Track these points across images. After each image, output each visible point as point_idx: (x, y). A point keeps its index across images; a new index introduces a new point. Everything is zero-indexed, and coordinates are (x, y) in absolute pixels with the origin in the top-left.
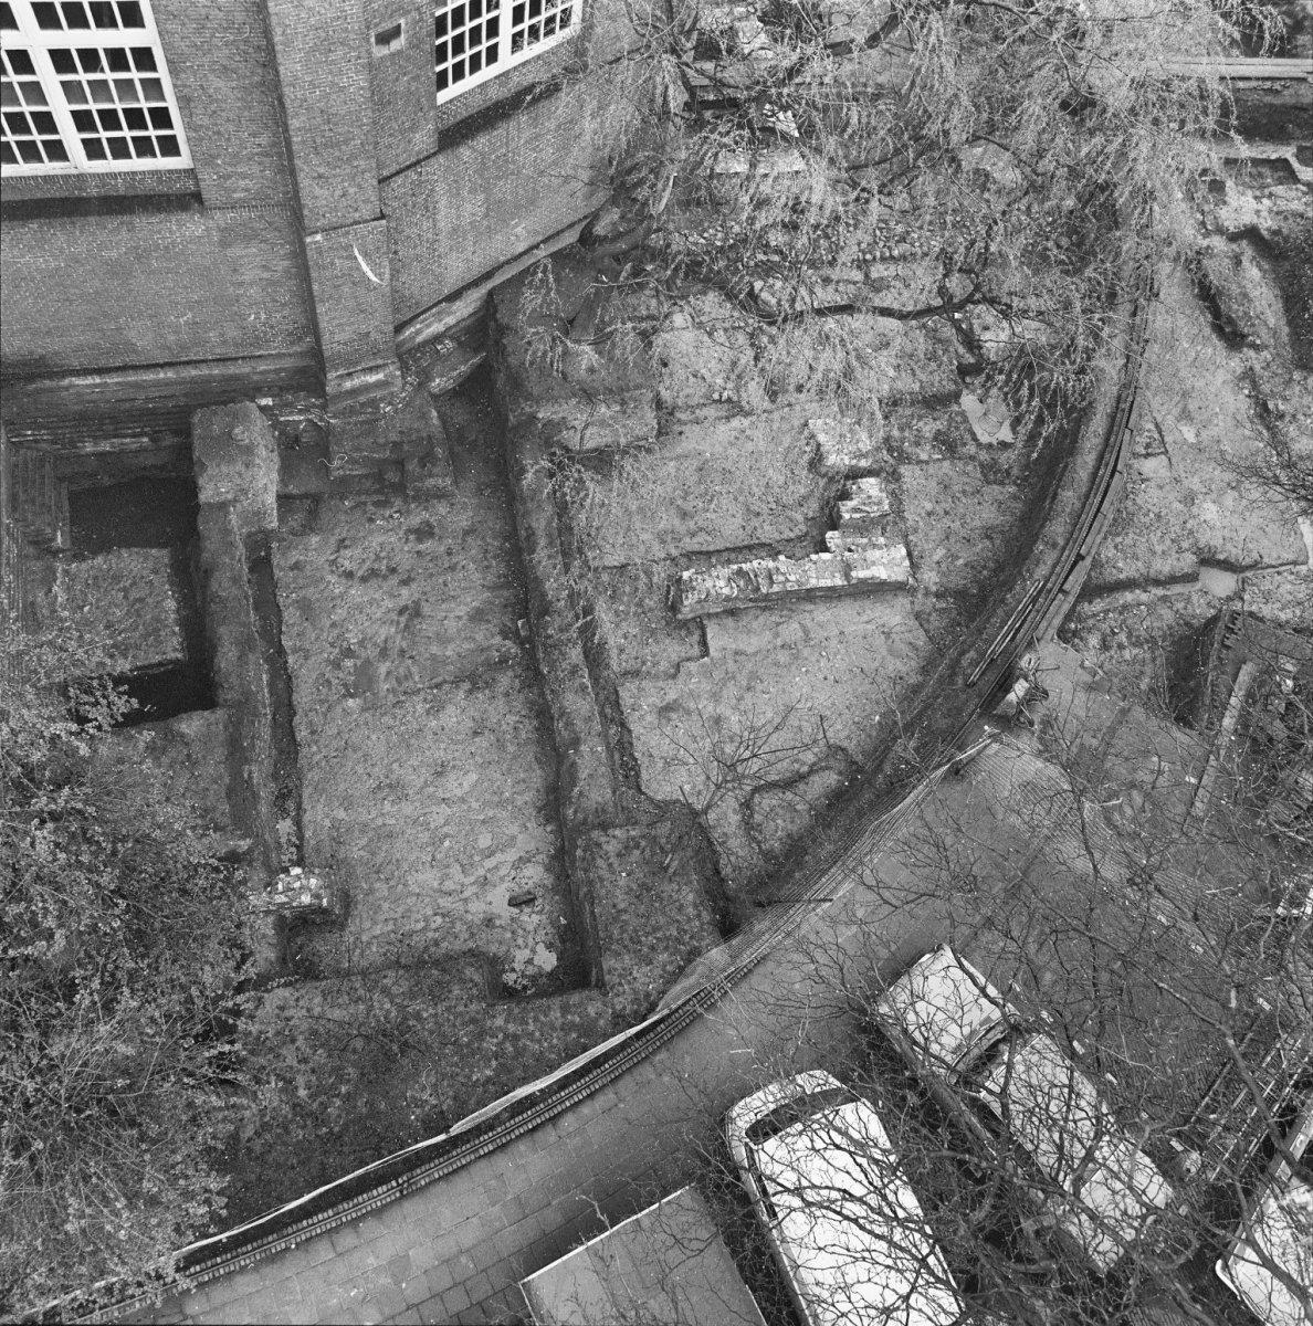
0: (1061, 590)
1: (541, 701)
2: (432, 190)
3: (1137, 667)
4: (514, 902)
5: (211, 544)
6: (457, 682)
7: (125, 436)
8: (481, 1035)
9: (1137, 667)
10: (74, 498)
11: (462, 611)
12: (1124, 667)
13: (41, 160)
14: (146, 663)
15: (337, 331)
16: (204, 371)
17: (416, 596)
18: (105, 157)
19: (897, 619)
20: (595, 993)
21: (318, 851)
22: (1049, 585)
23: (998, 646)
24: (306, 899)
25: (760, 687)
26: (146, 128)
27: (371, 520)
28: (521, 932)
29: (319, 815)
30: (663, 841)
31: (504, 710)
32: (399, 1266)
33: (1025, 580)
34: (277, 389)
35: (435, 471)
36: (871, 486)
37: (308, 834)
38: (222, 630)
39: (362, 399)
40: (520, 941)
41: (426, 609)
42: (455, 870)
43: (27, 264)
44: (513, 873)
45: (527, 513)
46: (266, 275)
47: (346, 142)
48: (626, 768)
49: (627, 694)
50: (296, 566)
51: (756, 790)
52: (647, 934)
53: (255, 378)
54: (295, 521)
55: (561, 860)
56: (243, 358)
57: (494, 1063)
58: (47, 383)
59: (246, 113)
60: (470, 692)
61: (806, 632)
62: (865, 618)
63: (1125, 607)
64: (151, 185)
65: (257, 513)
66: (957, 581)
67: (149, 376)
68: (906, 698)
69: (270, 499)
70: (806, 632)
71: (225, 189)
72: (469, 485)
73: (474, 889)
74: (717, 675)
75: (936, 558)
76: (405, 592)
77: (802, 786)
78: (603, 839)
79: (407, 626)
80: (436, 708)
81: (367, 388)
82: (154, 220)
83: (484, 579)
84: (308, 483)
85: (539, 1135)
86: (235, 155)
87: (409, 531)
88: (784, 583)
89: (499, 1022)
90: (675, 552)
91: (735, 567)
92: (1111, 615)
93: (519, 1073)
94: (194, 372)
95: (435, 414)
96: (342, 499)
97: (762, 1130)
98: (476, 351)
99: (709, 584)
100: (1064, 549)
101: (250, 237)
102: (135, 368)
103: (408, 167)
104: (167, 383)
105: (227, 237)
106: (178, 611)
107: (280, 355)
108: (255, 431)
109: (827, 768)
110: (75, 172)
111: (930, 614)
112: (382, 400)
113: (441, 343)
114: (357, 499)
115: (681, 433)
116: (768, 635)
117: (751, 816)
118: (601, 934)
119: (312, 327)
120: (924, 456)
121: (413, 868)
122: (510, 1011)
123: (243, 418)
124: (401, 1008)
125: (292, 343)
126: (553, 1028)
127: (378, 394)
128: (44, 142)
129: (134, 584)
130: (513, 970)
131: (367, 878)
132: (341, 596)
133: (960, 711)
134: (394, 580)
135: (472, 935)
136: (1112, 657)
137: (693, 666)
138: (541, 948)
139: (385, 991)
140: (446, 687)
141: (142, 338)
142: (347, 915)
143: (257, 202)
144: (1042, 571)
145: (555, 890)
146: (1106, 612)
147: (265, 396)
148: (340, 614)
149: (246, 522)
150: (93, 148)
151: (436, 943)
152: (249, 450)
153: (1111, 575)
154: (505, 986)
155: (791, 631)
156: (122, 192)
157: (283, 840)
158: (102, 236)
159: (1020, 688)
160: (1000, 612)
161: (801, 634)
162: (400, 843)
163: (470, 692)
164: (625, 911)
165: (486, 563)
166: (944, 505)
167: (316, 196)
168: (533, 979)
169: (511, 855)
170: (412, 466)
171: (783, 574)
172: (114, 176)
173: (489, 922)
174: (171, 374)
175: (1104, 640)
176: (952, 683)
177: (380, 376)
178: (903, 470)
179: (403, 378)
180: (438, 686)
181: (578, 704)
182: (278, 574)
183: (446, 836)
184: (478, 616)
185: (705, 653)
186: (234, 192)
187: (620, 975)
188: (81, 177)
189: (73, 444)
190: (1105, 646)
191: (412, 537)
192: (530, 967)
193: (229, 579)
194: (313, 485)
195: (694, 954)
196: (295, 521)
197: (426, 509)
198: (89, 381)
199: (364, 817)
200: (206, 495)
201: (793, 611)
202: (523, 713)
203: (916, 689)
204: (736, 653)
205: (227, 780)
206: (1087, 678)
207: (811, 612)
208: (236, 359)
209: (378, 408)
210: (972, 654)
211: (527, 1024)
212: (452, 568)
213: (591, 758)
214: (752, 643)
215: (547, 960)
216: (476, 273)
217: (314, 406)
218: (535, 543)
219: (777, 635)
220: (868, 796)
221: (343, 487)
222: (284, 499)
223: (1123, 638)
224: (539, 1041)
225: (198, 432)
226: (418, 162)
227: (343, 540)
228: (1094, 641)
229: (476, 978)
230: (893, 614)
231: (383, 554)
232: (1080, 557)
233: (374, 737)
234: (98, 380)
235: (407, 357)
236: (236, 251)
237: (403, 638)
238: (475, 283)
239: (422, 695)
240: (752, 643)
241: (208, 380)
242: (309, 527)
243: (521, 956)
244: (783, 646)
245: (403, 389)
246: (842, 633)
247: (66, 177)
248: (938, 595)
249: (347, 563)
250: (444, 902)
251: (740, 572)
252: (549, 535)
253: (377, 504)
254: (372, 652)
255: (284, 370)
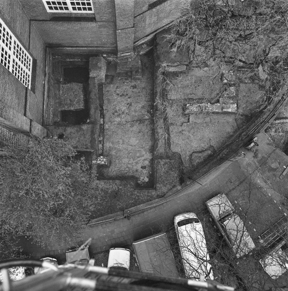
0: (268, 122)
1: (153, 128)
2: (146, 17)
3: (282, 137)
4: (142, 167)
5: (91, 86)
6: (137, 121)
7: (76, 59)
8: (132, 195)
9: (282, 137)
10: (65, 69)
11: (140, 106)
12: (279, 137)
13: (63, 10)
14: (77, 108)
15: (121, 46)
16: (93, 48)
17: (131, 101)
18: (76, 10)
19: (231, 120)
20: (154, 191)
21: (106, 152)
22: (266, 120)
23: (251, 132)
24: (103, 163)
25: (199, 131)
26: (85, 6)
27: (124, 83)
28: (142, 173)
29: (108, 145)
30: (172, 163)
31: (146, 129)
32: (113, 232)
33: (261, 118)
34: (108, 53)
35: (138, 74)
36: (232, 89)
37: (105, 148)
38: (92, 105)
39: (125, 57)
40: (142, 175)
41: (133, 104)
42: (132, 159)
43: (59, 29)
44: (143, 162)
45: (156, 87)
46: (108, 33)
47: (128, 14)
48: (168, 143)
49: (171, 128)
50: (108, 91)
51: (193, 152)
52: (166, 181)
53: (103, 50)
54: (109, 80)
55: (152, 161)
56: (101, 47)
57: (134, 200)
58: (61, 48)
59: (107, 6)
60: (139, 123)
61: (211, 120)
62: (224, 119)
63: (283, 123)
64: (85, 16)
65: (101, 79)
66: (246, 113)
67: (82, 48)
68: (229, 138)
69: (104, 77)
70: (211, 120)
71: (101, 18)
72: (145, 77)
73: (135, 164)
74: (190, 127)
75: (243, 107)
76: (129, 100)
77: (203, 153)
78: (161, 161)
79: (128, 107)
80: (132, 126)
81: (126, 56)
82: (85, 23)
83: (145, 99)
84: (112, 73)
85: (140, 214)
86: (104, 13)
87: (131, 86)
88: (208, 110)
89: (136, 193)
90: (186, 98)
91: (198, 105)
92: (279, 124)
93: (138, 202)
94: (90, 49)
95: (140, 62)
96: (119, 77)
97: (181, 223)
98: (151, 46)
99: (192, 108)
100: (271, 112)
101: (105, 27)
102: (79, 47)
103: (141, 14)
104: (85, 50)
105: (100, 27)
106: (83, 98)
107: (109, 47)
108: (103, 64)
109: (210, 150)
110: (70, 12)
111: (239, 119)
112: (129, 58)
113: (143, 45)
114: (122, 78)
115: (193, 70)
116: (203, 120)
117: (191, 157)
118: (157, 180)
119: (116, 42)
120: (246, 82)
121: (124, 158)
122: (138, 191)
123: (100, 60)
124: (118, 187)
125: (111, 45)
126: (145, 196)
127: (128, 57)
128: (64, 7)
129: (75, 91)
130: (140, 180)
131: (115, 158)
132: (116, 99)
133: (239, 145)
134: (127, 97)
135: (133, 173)
136: (276, 134)
137: (185, 124)
138: (146, 177)
139: (116, 184)
140: (135, 122)
141: (81, 42)
142: (110, 165)
143: (107, 21)
144: (265, 116)
145: (150, 166)
146: (278, 123)
147: (105, 54)
148: (115, 103)
149: (98, 81)
150: (74, 9)
151: (126, 173)
152: (100, 68)
153: (282, 116)
154: (138, 183)
155: (208, 119)
156: (79, 16)
157: (100, 148)
158: (74, 25)
159: (252, 144)
160: (253, 124)
161: (210, 120)
162: (122, 153)
163: (139, 123)
164: (163, 176)
165: (146, 96)
166: (248, 94)
167: (120, 24)
168: (144, 183)
169: (143, 158)
170: (134, 73)
171: (209, 108)
172: (78, 14)
173: (137, 171)
174: (86, 48)
175: (276, 130)
176: (239, 139)
177: (129, 54)
178: (241, 85)
179: (134, 53)
180: (133, 121)
181: (160, 131)
182: (104, 92)
183: (131, 152)
184: (143, 107)
185: (189, 122)
186: (103, 19)
187: (159, 188)
188: (71, 14)
189: (65, 59)
190: (276, 132)
191: (132, 88)
192: (143, 181)
193: (94, 95)
194: (113, 73)
195: (174, 186)
196: (109, 80)
197: (135, 82)
198: (69, 48)
199: (116, 146)
200: (91, 75)
201: (209, 115)
202: (149, 129)
203: (232, 136)
204: (195, 123)
205: (90, 139)
206: (268, 142)
207: (213, 116)
208: (100, 47)
209: (128, 60)
210: (245, 133)
211: (141, 194)
212: (139, 96)
213: (161, 143)
214: (199, 121)
215: (147, 180)
216: (153, 31)
217: (115, 57)
218: (157, 94)
219: (204, 120)
220: (215, 160)
221: (119, 75)
222: (107, 76)
223: (280, 130)
224: (143, 198)
225: (90, 62)
226: (143, 13)
227: (118, 86)
228: (274, 130)
229: (133, 184)
230: (231, 119)
231: (125, 91)
232: (274, 115)
233: (119, 130)
234: (71, 48)
235: (135, 49)
236: (102, 29)
237: (128, 110)
238: (153, 33)
239: (130, 123)
240: (199, 121)
241: (94, 50)
242: (111, 83)
243: (142, 178)
244: (205, 123)
245: (134, 56)
246: (218, 121)
247: (68, 13)
248: (242, 115)
249: (118, 92)
250: (129, 166)
251: (199, 106)
252: (160, 93)
253: (126, 79)
254: (121, 112)
255: (109, 49)
